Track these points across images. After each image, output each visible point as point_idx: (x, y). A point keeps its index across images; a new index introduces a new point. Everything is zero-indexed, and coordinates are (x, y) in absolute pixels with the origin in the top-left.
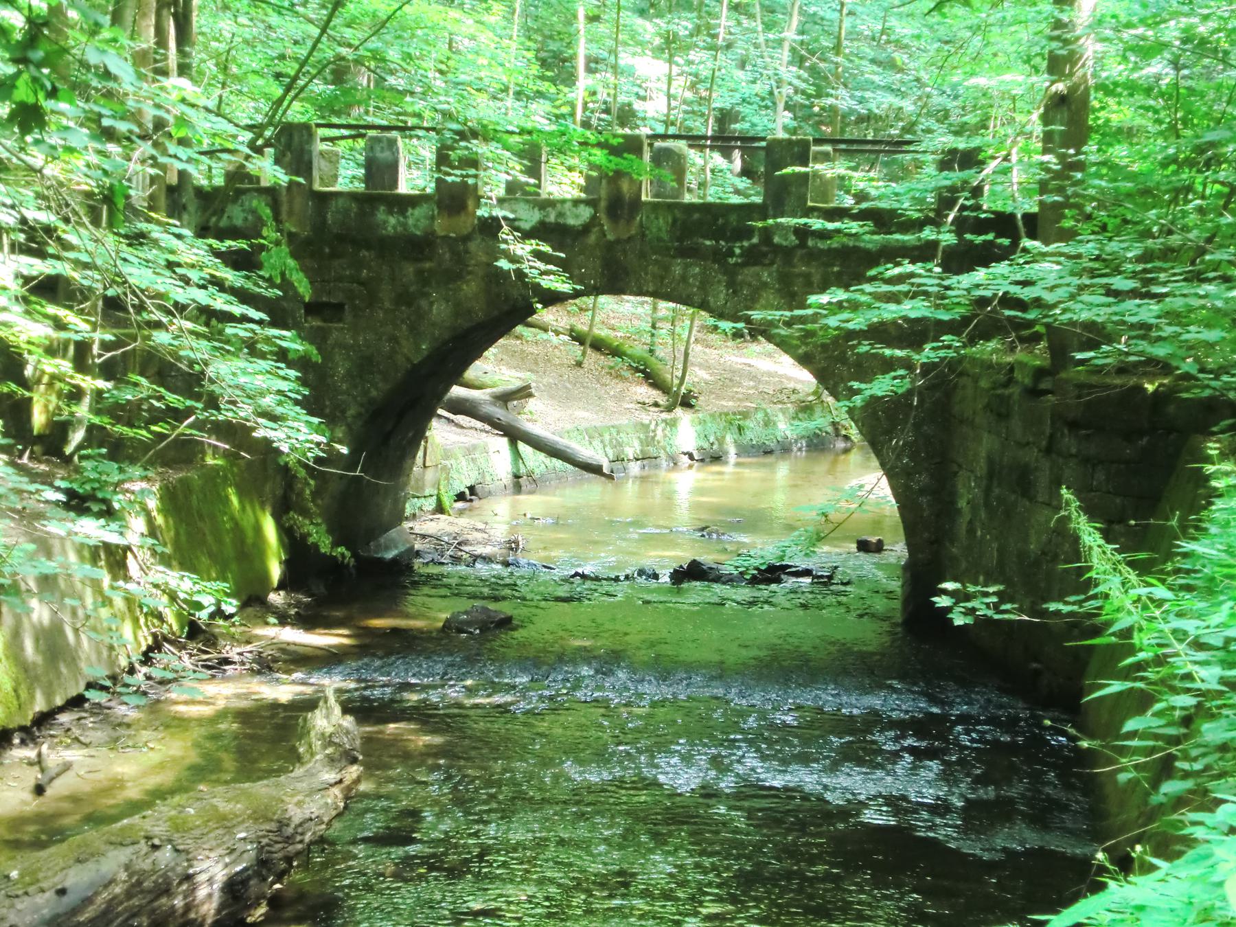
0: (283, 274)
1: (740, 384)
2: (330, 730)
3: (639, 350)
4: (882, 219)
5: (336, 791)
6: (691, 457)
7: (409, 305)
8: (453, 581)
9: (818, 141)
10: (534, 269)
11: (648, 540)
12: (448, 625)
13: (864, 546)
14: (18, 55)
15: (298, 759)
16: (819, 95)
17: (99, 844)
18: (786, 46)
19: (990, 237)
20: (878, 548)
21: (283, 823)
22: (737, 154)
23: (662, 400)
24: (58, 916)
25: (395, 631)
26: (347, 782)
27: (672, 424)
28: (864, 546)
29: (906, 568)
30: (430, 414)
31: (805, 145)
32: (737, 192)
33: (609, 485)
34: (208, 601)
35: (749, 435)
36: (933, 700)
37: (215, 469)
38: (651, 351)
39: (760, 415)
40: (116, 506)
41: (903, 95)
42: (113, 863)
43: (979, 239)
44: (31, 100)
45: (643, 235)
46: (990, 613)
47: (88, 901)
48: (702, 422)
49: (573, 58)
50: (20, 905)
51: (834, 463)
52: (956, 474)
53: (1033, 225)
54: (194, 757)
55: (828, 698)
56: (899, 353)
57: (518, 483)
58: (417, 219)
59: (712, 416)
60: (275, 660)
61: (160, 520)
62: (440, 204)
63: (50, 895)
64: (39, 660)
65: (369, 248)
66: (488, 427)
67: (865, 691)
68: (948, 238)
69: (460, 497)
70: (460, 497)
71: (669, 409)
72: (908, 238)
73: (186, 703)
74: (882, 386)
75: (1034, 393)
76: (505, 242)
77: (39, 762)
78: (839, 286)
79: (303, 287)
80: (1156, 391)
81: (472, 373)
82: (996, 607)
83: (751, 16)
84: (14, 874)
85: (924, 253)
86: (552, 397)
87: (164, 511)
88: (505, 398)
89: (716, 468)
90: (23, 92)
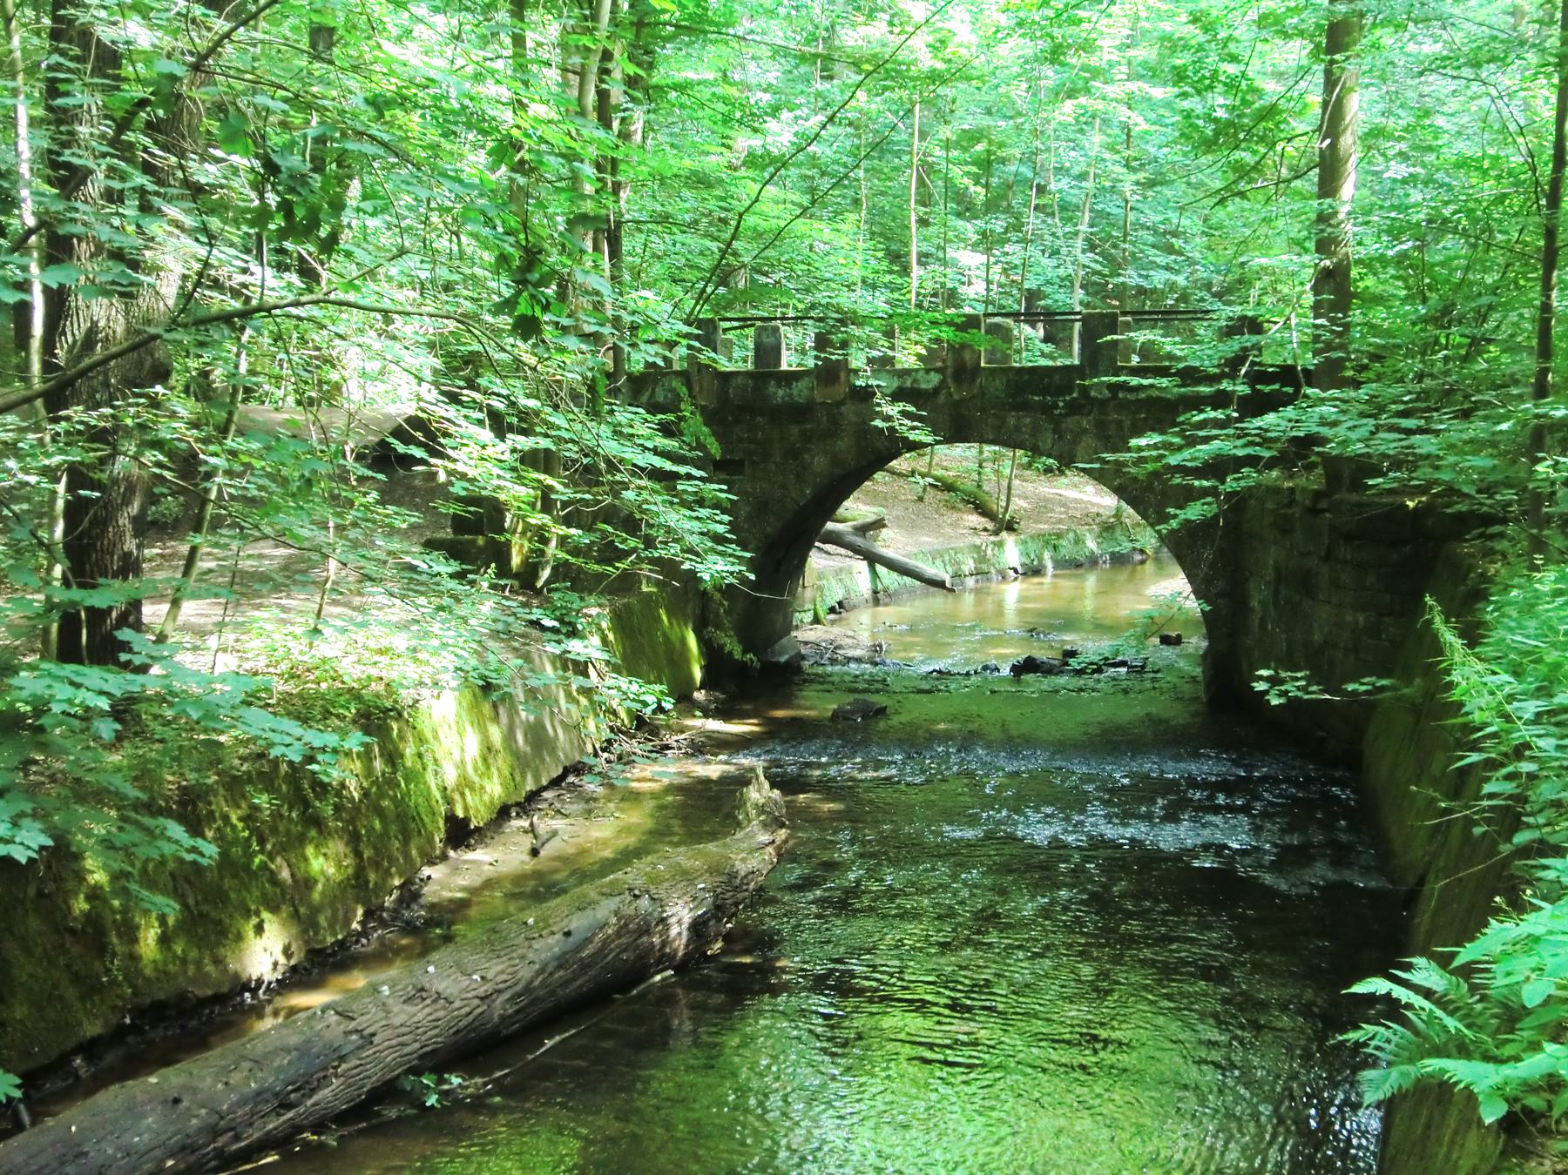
0: (698, 439)
1: (1052, 511)
2: (762, 801)
3: (969, 486)
4: (1190, 375)
5: (770, 849)
6: (1016, 571)
7: (795, 458)
8: (836, 679)
9: (1124, 314)
10: (904, 427)
11: (989, 641)
12: (836, 714)
13: (1166, 640)
14: (518, 277)
15: (739, 825)
16: (1111, 276)
17: (593, 895)
18: (1081, 236)
19: (1276, 387)
20: (1175, 641)
21: (732, 876)
22: (1040, 325)
23: (990, 526)
24: (565, 953)
25: (794, 720)
26: (778, 842)
27: (1000, 545)
28: (1166, 640)
29: (1204, 657)
30: (810, 546)
31: (1114, 317)
32: (1043, 355)
33: (950, 596)
34: (651, 699)
35: (1063, 551)
36: (1236, 763)
37: (650, 594)
38: (979, 486)
39: (1071, 535)
40: (580, 627)
41: (1178, 272)
42: (605, 910)
43: (1267, 389)
44: (530, 313)
45: (983, 394)
46: (1299, 694)
47: (588, 941)
48: (1024, 542)
49: (908, 254)
50: (536, 945)
51: (1134, 571)
52: (1247, 580)
53: (1310, 377)
54: (649, 824)
55: (1149, 766)
56: (1205, 483)
57: (876, 598)
58: (800, 390)
59: (1032, 537)
60: (703, 743)
61: (611, 637)
62: (818, 377)
63: (558, 936)
64: (528, 749)
65: (762, 415)
66: (850, 553)
67: (1178, 758)
68: (1242, 389)
69: (832, 610)
70: (832, 610)
71: (996, 533)
72: (1204, 389)
73: (638, 780)
74: (1194, 512)
75: (1314, 511)
76: (879, 405)
77: (532, 829)
78: (1153, 430)
79: (715, 449)
80: (1415, 509)
81: (841, 511)
82: (1304, 689)
83: (1053, 215)
84: (531, 921)
85: (1221, 400)
86: (900, 527)
87: (614, 629)
88: (863, 529)
89: (1036, 580)
90: (523, 308)
